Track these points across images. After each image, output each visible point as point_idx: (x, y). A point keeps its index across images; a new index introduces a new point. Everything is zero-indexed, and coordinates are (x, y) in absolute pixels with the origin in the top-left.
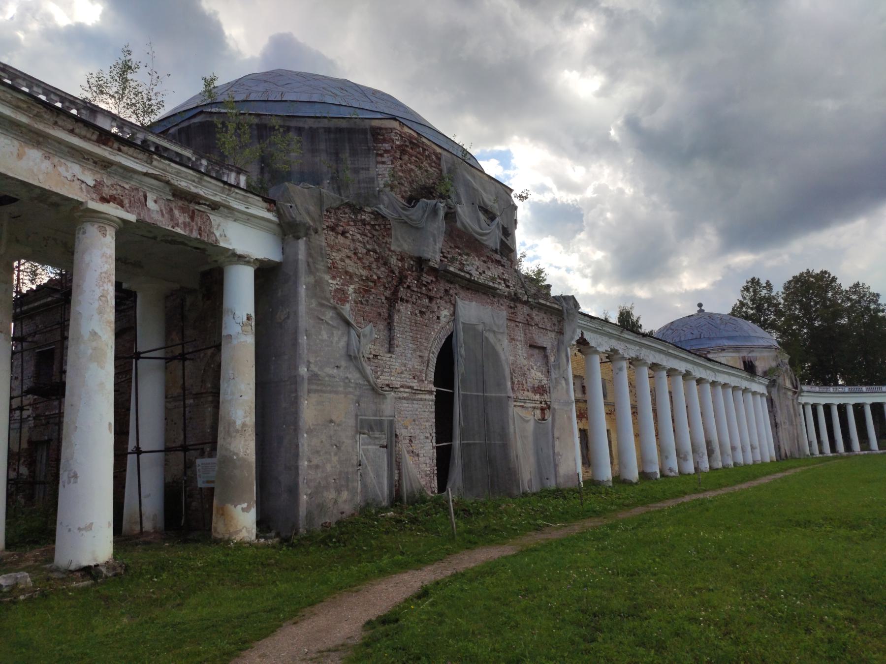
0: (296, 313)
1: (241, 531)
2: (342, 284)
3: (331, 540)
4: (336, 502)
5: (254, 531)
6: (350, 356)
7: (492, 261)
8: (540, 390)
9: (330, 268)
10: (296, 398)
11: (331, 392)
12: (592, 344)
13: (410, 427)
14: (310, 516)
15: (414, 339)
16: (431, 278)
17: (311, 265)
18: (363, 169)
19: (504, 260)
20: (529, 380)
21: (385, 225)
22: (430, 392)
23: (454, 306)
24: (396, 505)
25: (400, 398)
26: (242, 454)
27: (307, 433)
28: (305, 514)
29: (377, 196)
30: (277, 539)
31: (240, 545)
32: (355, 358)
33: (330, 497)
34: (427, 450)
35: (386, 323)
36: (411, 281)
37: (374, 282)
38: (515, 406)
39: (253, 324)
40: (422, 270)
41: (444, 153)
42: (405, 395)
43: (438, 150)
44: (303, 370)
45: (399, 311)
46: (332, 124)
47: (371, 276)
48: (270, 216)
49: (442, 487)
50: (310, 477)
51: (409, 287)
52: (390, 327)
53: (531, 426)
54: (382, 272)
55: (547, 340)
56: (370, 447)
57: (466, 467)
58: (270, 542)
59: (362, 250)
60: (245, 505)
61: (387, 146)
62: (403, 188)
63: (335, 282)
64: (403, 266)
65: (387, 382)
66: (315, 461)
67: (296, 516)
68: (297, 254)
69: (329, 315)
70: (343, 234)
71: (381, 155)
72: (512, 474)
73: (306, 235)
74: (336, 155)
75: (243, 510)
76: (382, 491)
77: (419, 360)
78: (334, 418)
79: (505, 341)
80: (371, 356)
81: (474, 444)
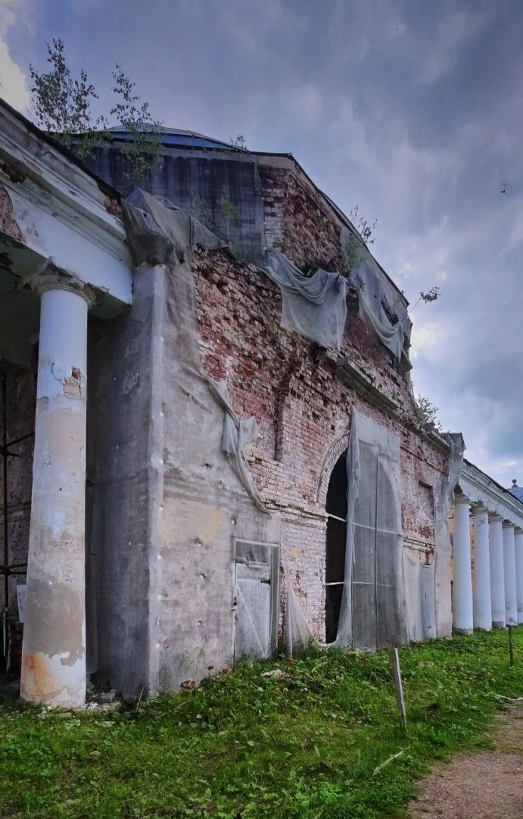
0: (149, 377)
1: (59, 692)
2: (217, 351)
3: (194, 715)
4: (202, 653)
5: (82, 692)
6: (225, 453)
7: (389, 376)
8: (426, 532)
9: (200, 322)
10: (147, 501)
11: (197, 499)
12: (465, 492)
13: (297, 559)
14: (164, 674)
15: (306, 447)
16: (327, 374)
17: (174, 310)
18: (246, 221)
19: (399, 379)
20: (417, 519)
21: (275, 293)
22: (322, 518)
23: (350, 416)
24: (281, 659)
25: (287, 521)
26: (61, 579)
27: (161, 554)
28: (157, 670)
29: (263, 258)
30: (118, 703)
31: (56, 717)
32: (233, 456)
33: (195, 645)
34: (317, 590)
35: (272, 421)
36: (304, 368)
37: (258, 362)
38: (404, 546)
39: (84, 384)
40: (316, 362)
41: (344, 229)
42: (293, 518)
43: (338, 222)
44: (157, 462)
45: (289, 406)
46: (209, 156)
47: (255, 354)
48: (112, 221)
49: (331, 636)
50: (165, 617)
51: (302, 378)
52: (277, 427)
53: (417, 569)
54: (269, 352)
55: (433, 478)
56: (249, 581)
57: (356, 610)
58: (106, 707)
59: (243, 314)
60: (66, 655)
61: (279, 192)
62: (296, 254)
63: (207, 345)
64: (295, 352)
65: (272, 498)
66: (173, 596)
67: (145, 674)
68: (151, 287)
69: (198, 389)
70: (221, 285)
71: (271, 205)
72: (398, 620)
73: (167, 261)
74: (212, 200)
75: (63, 662)
76: (262, 642)
77: (311, 476)
78: (201, 537)
79: (398, 471)
80: (253, 459)
81: (365, 585)
